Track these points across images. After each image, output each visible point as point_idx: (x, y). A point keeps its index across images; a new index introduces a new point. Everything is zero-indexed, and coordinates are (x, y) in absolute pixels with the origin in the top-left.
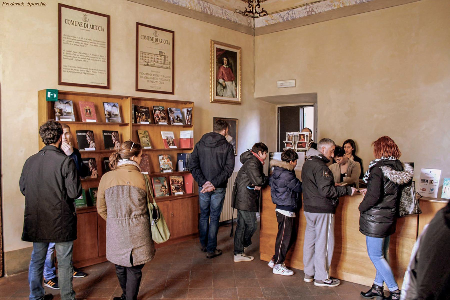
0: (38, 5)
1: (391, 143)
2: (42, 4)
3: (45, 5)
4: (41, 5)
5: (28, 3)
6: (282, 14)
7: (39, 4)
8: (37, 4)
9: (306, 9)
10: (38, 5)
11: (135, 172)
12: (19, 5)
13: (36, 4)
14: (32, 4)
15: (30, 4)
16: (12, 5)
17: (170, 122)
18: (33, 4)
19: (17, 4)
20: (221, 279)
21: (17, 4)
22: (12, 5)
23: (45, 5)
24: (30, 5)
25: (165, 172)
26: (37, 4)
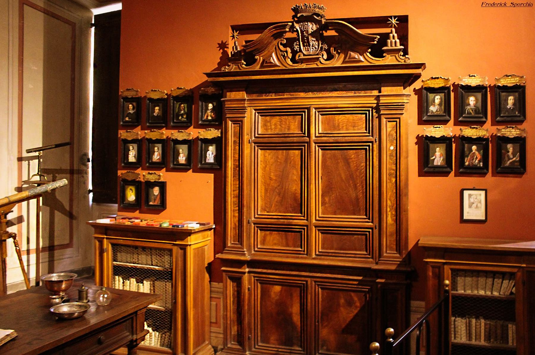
0: (523, 5)
4: (527, 6)
5: (511, 3)
7: (524, 5)
8: (522, 5)
13: (521, 4)
14: (516, 4)
15: (513, 4)
16: (492, 5)
18: (517, 5)
19: (499, 5)
21: (499, 5)
22: (492, 5)
24: (514, 6)
26: (522, 5)
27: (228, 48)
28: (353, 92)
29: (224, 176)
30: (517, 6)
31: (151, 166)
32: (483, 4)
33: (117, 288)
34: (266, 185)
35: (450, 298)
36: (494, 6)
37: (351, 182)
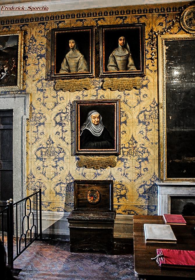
0: (40, 9)
1: (178, 101)
2: (44, 8)
3: (47, 9)
4: (43, 10)
5: (29, 7)
6: (156, 39)
7: (41, 9)
8: (39, 9)
9: (20, 164)
10: (40, 9)
11: (141, 104)
12: (19, 10)
14: (33, 8)
15: (30, 8)
16: (11, 9)
17: (2, 219)
18: (34, 9)
19: (17, 9)
20: (62, 244)
21: (17, 9)
22: (11, 9)
23: (47, 9)
24: (31, 10)
25: (179, 68)
27: (166, 57)
28: (98, 255)
29: (108, 28)
30: (34, 10)
31: (55, 34)
32: (2, 8)
33: (158, 215)
34: (48, 41)
35: (16, 34)
36: (13, 10)
37: (183, 45)
